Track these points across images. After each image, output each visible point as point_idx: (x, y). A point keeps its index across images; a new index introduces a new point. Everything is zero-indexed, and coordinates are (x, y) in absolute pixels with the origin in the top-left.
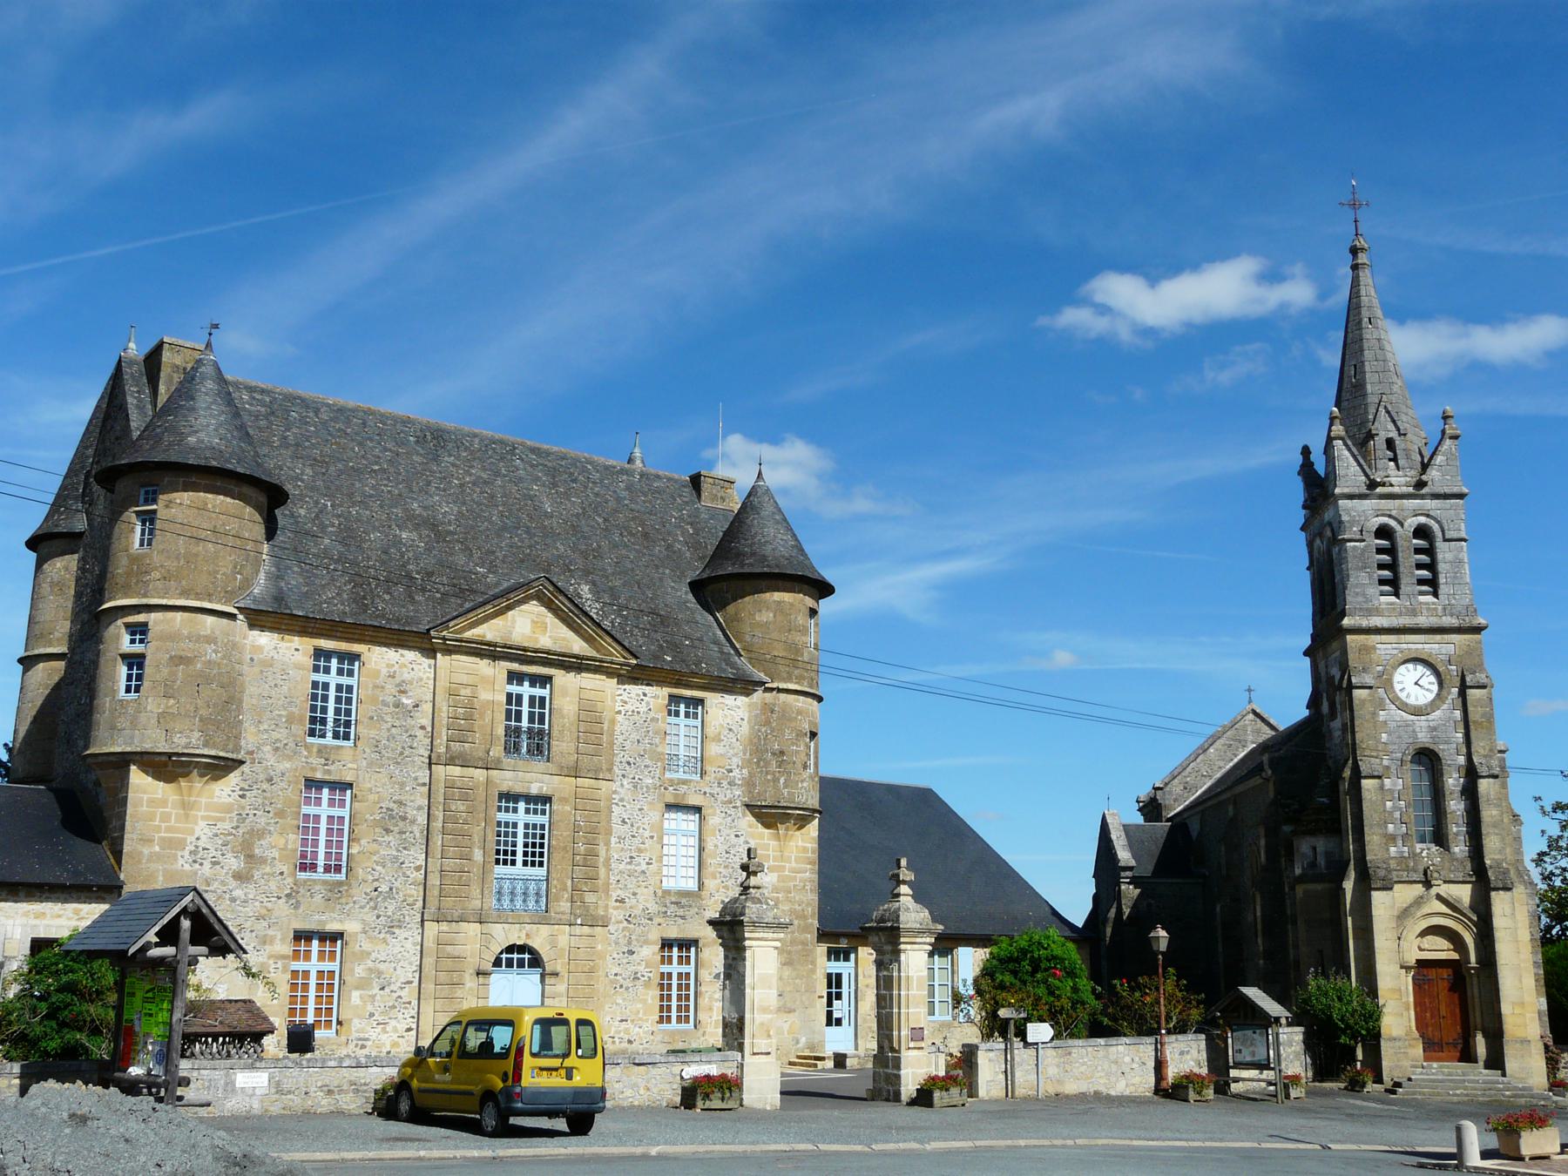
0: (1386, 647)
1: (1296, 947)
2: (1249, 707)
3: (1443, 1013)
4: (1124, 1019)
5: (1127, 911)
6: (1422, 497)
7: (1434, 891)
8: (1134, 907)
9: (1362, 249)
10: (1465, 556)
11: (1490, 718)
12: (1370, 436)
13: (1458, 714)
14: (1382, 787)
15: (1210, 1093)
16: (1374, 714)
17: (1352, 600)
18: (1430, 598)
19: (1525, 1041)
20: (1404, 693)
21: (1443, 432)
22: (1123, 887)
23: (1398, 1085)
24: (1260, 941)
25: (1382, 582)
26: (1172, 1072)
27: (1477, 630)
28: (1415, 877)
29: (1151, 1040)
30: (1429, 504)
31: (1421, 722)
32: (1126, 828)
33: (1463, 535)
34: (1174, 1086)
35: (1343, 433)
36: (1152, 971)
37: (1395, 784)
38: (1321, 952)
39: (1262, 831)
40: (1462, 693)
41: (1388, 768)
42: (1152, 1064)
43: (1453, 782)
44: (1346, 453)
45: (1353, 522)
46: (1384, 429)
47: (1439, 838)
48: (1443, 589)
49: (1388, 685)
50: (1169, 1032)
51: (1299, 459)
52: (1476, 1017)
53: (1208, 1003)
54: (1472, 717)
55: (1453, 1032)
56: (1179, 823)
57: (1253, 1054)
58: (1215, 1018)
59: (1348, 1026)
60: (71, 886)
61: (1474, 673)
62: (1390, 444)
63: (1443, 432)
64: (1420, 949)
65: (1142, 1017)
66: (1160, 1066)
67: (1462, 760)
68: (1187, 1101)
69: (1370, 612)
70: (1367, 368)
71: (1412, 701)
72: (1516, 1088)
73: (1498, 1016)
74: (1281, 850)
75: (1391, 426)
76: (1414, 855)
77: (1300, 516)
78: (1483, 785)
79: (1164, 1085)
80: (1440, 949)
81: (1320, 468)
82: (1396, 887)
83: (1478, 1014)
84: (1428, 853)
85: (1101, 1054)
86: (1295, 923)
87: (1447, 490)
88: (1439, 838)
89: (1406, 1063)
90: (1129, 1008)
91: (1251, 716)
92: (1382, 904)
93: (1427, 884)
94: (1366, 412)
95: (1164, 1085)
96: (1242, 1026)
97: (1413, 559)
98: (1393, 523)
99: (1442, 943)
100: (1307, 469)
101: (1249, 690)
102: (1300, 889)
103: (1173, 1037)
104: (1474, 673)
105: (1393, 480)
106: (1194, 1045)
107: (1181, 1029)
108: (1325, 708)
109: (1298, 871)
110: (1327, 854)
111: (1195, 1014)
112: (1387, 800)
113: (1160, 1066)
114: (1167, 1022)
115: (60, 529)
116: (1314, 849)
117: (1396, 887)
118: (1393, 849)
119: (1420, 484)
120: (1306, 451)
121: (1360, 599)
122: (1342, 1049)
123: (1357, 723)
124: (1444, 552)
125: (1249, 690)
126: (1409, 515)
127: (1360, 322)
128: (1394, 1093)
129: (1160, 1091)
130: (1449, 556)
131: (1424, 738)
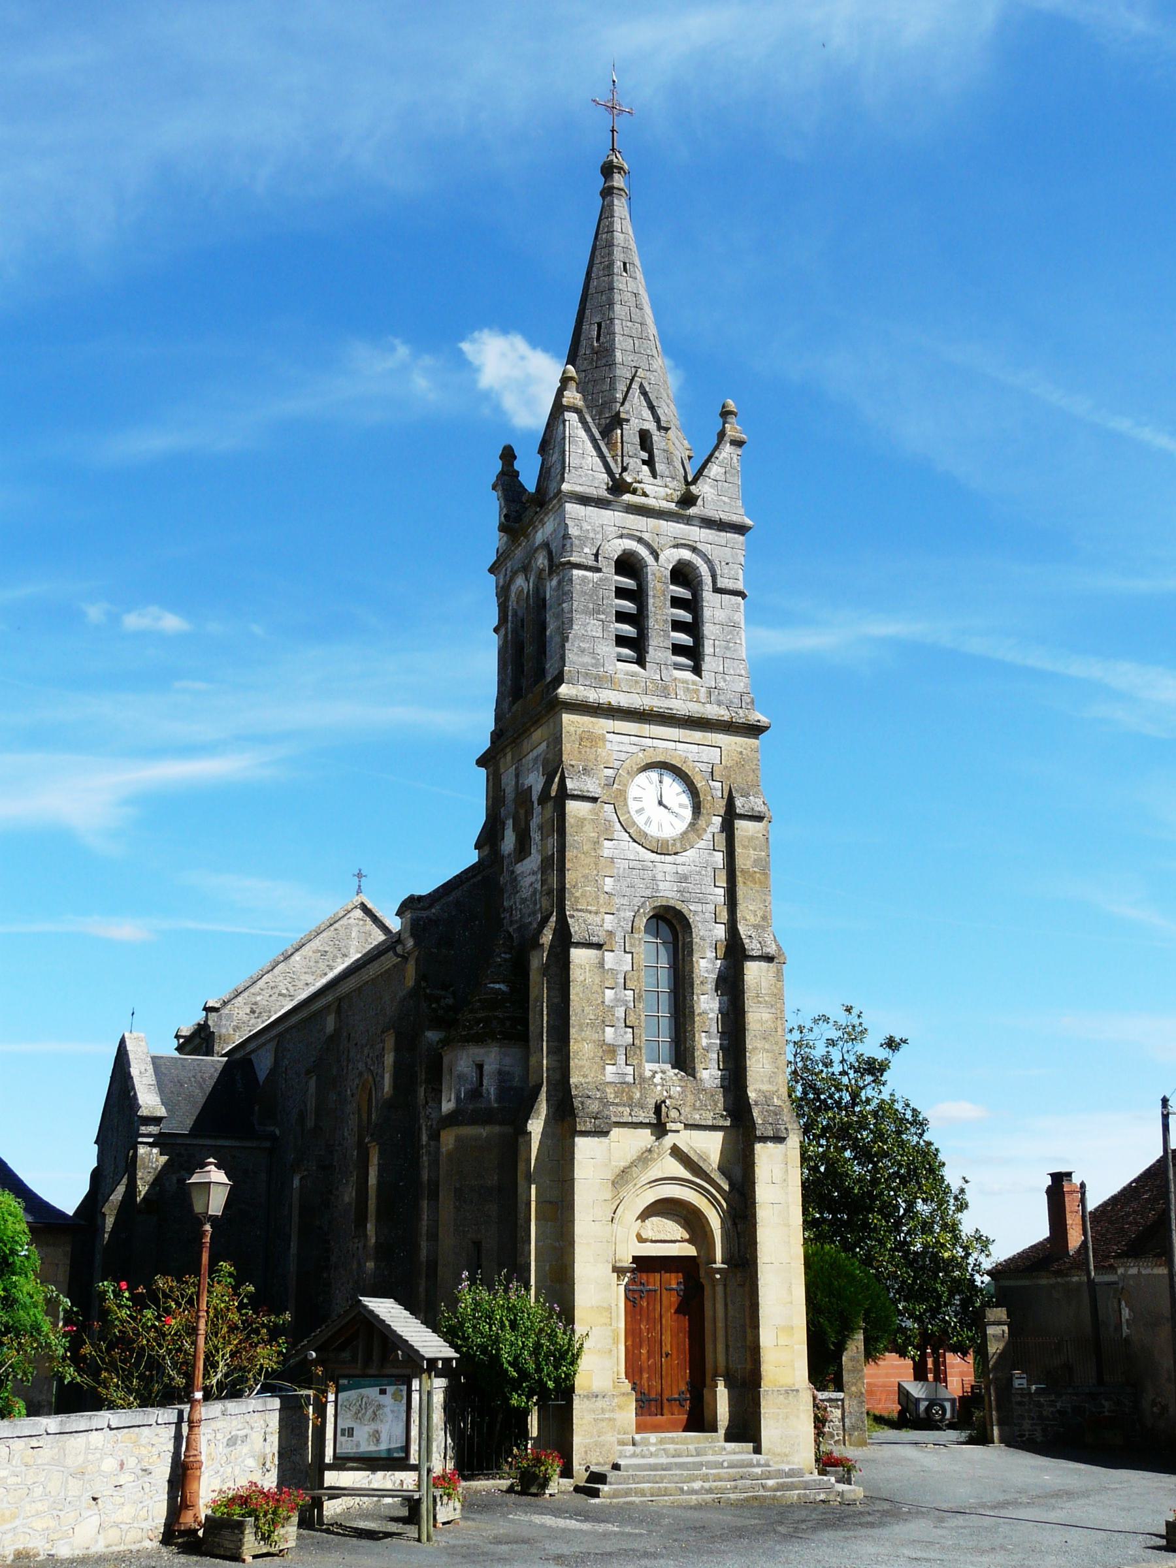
0: (620, 742)
1: (433, 1237)
2: (357, 900)
3: (667, 1348)
4: (112, 1367)
5: (143, 1189)
6: (688, 520)
7: (669, 1140)
9: (620, 169)
10: (740, 617)
11: (764, 866)
12: (617, 421)
13: (719, 858)
14: (601, 964)
15: (289, 1534)
16: (597, 843)
17: (574, 659)
18: (689, 676)
19: (792, 1391)
20: (635, 829)
21: (722, 435)
22: (142, 1150)
23: (600, 1478)
24: (370, 1227)
25: (621, 641)
26: (209, 1492)
27: (754, 730)
29: (168, 1415)
30: (696, 533)
31: (665, 866)
32: (155, 1060)
33: (740, 586)
34: (212, 1524)
35: (580, 403)
36: (186, 1266)
37: (619, 962)
38: (477, 1245)
39: (390, 1041)
40: (728, 828)
41: (610, 933)
42: (163, 1471)
43: (706, 965)
44: (582, 433)
45: (583, 540)
46: (638, 417)
47: (683, 1059)
48: (708, 664)
49: (619, 801)
50: (207, 1397)
51: (498, 466)
52: (717, 1353)
53: (296, 1334)
54: (740, 862)
55: (677, 1384)
56: (240, 1061)
57: (376, 1436)
58: (306, 1363)
59: (524, 1374)
61: (746, 795)
62: (645, 439)
63: (722, 435)
64: (641, 1239)
65: (155, 1365)
66: (182, 1475)
67: (720, 932)
68: (237, 1558)
69: (600, 681)
70: (618, 328)
71: (653, 831)
72: (780, 1473)
73: (754, 1351)
74: (421, 1071)
75: (647, 414)
76: (641, 1080)
77: (491, 541)
78: (753, 972)
79: (187, 1520)
81: (529, 481)
82: (615, 1132)
83: (721, 1347)
84: (663, 1078)
85: (46, 1454)
86: (434, 1196)
87: (725, 517)
88: (683, 1059)
89: (611, 1438)
90: (124, 1341)
91: (359, 913)
92: (592, 1158)
93: (660, 1129)
94: (613, 388)
95: (187, 1520)
96: (359, 1379)
97: (667, 611)
98: (643, 552)
99: (672, 1229)
100: (508, 481)
101: (360, 875)
102: (448, 1139)
103: (216, 1408)
104: (746, 795)
105: (648, 489)
106: (257, 1421)
107: (232, 1390)
108: (509, 842)
109: (447, 1106)
110: (502, 1076)
111: (266, 1357)
112: (609, 987)
113: (182, 1475)
114: (206, 1375)
116: (480, 1067)
117: (615, 1132)
118: (610, 1069)
119: (688, 500)
120: (508, 455)
121: (587, 659)
122: (507, 1418)
123: (569, 855)
124: (714, 608)
125: (360, 875)
126: (667, 544)
127: (611, 265)
128: (595, 1493)
129: (175, 1535)
130: (720, 615)
131: (668, 893)
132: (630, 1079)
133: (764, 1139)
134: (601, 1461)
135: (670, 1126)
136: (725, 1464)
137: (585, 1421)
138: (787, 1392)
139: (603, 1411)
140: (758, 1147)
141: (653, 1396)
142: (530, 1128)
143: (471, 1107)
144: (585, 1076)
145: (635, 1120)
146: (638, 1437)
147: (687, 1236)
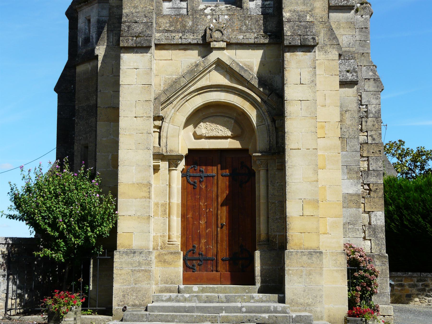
7: (214, 56)
8: (191, 165)
28: (190, 38)
55: (218, 246)
60: (193, 260)
64: (197, 137)
80: (218, 137)
93: (205, 46)
115: (228, 119)
132: (184, 11)
133: (293, 48)
134: (137, 302)
135: (214, 44)
136: (244, 310)
137: (123, 272)
138: (310, 253)
139: (140, 264)
140: (287, 55)
141: (210, 256)
142: (97, 52)
143: (84, 51)
144: (136, 7)
145: (184, 41)
146: (182, 286)
147: (229, 133)
